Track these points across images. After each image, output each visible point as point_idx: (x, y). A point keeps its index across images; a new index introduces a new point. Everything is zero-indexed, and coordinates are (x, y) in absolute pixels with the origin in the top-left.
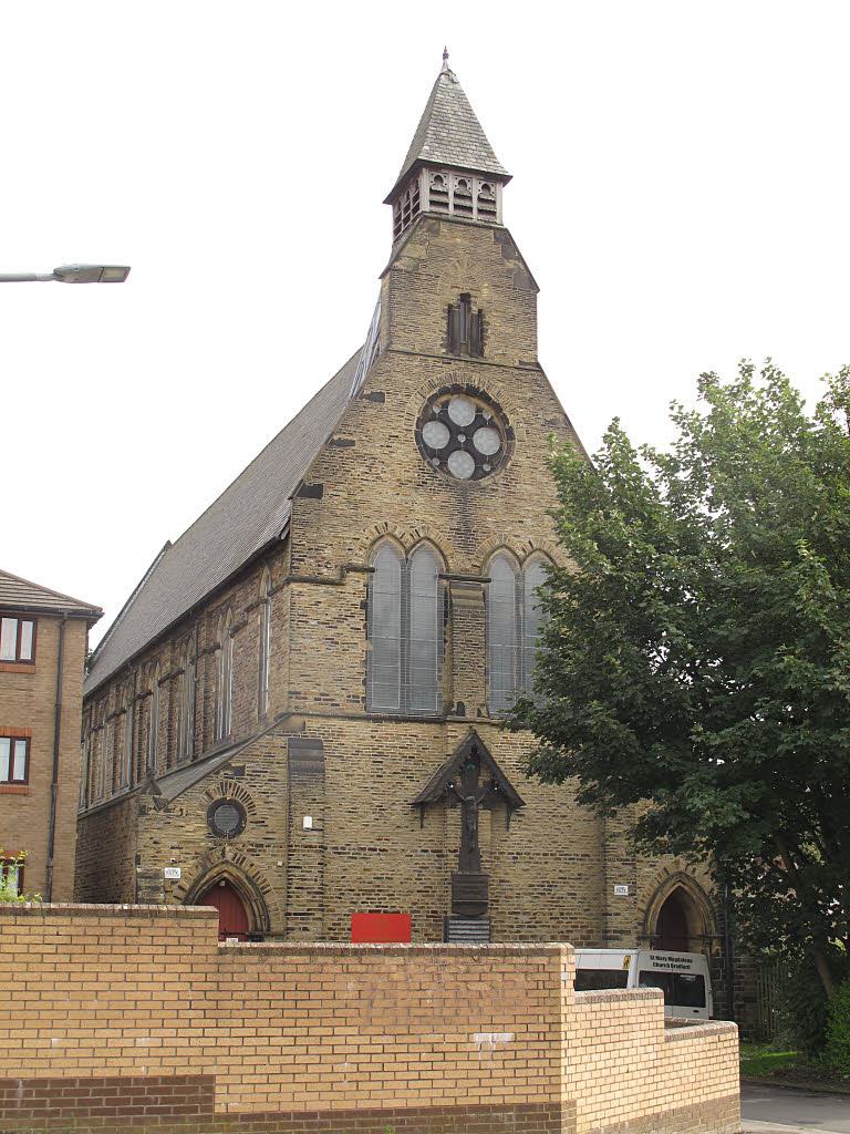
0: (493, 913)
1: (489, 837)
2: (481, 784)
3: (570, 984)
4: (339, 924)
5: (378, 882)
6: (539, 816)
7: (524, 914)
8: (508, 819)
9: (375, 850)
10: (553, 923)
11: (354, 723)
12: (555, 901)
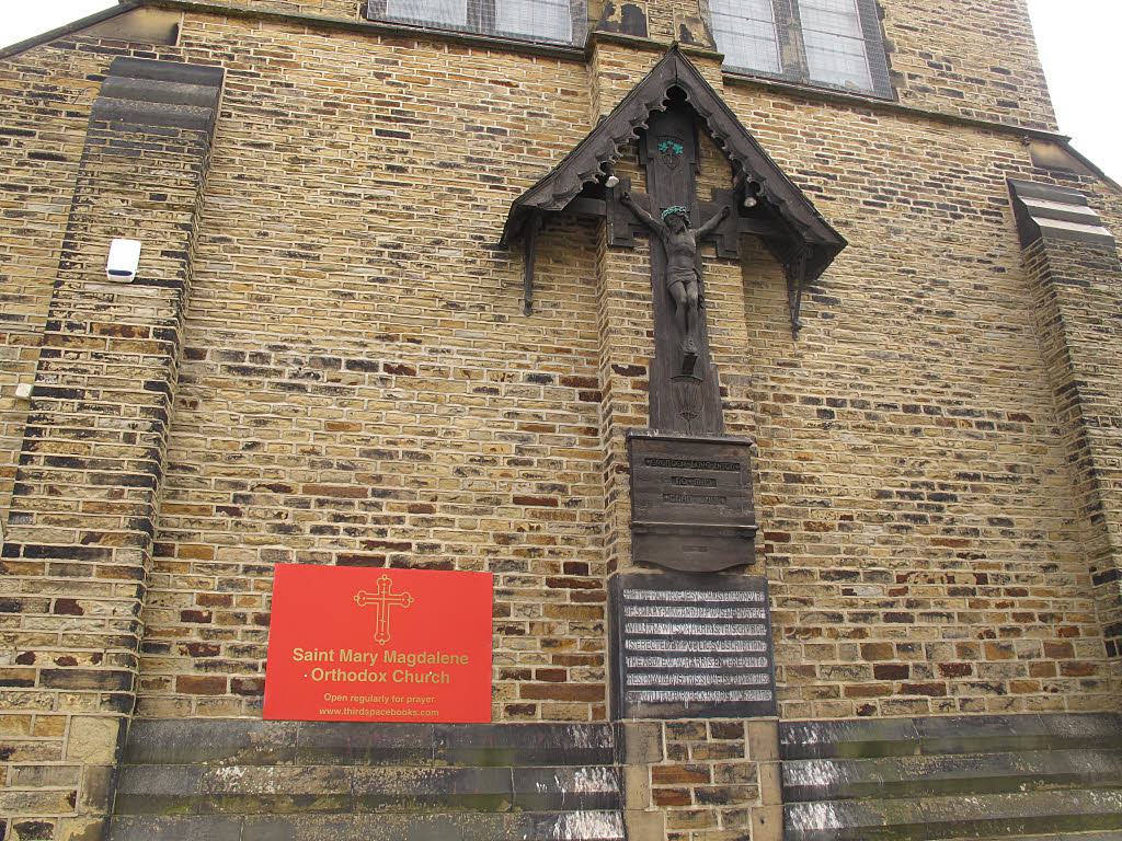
0: (775, 576)
1: (743, 334)
2: (704, 194)
3: (555, 653)
4: (227, 601)
5: (375, 467)
6: (879, 306)
7: (871, 577)
8: (794, 309)
9: (372, 367)
10: (960, 605)
11: (328, 42)
12: (958, 541)
